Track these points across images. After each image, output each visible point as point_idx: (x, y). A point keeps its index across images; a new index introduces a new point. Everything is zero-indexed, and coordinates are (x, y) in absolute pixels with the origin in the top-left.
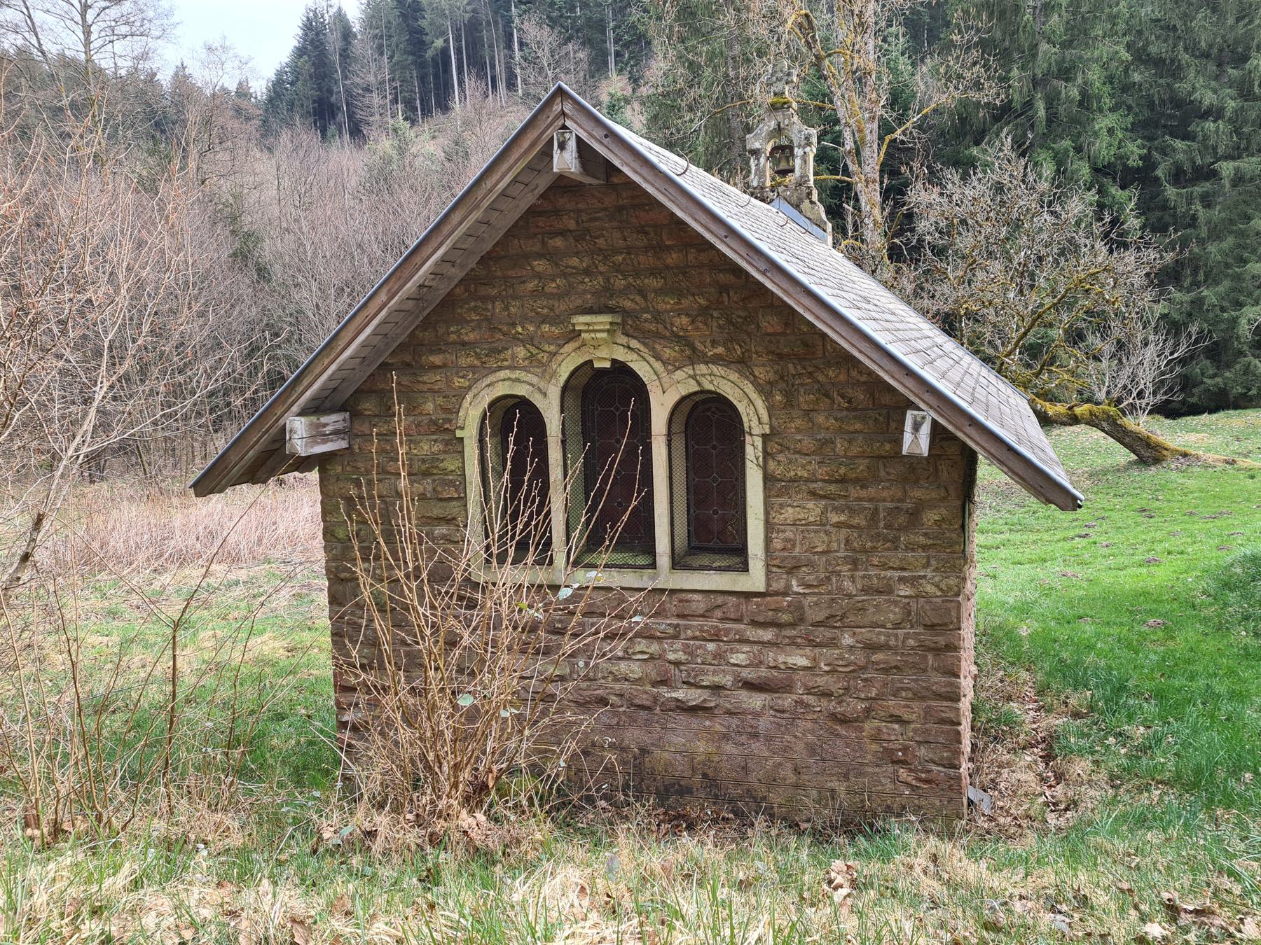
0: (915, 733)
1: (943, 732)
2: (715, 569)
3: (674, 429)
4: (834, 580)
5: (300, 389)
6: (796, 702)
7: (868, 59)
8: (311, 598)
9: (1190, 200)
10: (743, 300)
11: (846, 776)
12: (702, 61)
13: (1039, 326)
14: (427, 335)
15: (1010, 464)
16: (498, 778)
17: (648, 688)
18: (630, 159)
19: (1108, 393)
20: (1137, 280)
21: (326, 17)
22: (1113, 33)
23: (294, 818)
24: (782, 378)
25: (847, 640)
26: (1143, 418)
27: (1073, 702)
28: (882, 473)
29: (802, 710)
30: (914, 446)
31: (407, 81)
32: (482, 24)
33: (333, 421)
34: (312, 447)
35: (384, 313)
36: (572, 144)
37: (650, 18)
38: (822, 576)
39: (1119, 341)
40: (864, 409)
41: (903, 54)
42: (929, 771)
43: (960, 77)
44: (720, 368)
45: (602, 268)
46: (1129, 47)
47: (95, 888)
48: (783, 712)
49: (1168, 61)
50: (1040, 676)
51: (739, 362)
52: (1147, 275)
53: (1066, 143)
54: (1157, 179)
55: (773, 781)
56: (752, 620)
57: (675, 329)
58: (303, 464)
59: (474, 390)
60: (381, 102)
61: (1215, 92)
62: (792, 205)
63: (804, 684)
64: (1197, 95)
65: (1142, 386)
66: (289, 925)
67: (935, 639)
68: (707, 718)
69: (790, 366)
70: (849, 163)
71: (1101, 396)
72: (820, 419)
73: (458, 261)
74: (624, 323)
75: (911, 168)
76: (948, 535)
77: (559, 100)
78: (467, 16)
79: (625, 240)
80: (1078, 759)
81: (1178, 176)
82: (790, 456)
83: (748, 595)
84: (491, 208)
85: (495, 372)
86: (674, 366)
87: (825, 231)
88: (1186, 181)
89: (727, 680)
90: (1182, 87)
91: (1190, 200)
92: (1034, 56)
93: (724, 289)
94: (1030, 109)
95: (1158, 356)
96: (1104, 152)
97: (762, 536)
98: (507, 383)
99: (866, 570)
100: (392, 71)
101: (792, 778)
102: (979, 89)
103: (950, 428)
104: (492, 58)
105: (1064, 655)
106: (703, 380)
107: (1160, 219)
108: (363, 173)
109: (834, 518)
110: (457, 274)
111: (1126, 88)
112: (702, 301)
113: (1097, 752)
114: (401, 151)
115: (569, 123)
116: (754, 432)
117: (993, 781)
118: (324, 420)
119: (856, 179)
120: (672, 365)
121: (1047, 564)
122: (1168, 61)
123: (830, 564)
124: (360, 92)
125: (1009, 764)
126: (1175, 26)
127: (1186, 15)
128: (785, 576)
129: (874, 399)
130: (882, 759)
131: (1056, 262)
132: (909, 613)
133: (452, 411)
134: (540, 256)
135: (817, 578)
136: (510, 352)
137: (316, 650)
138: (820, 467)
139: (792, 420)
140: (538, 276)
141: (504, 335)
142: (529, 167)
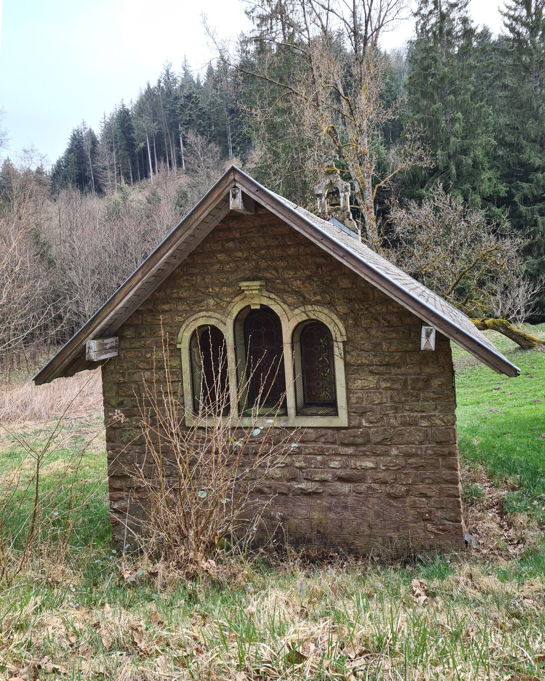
0: (435, 503)
1: (450, 502)
2: (320, 415)
3: (295, 340)
4: (385, 419)
6: (368, 487)
7: (365, 147)
8: (82, 438)
9: (533, 212)
10: (330, 271)
11: (398, 529)
12: (280, 151)
13: (464, 278)
14: (161, 295)
15: (479, 353)
16: (220, 539)
17: (285, 483)
18: (270, 202)
19: (502, 312)
20: (512, 253)
21: (83, 133)
22: (486, 132)
23: (102, 566)
24: (352, 311)
25: (394, 452)
26: (520, 325)
27: (510, 481)
28: (408, 360)
29: (371, 492)
30: (427, 345)
31: (125, 164)
33: (110, 341)
34: (100, 356)
35: (140, 284)
36: (239, 195)
37: (253, 130)
38: (379, 416)
39: (505, 285)
40: (397, 326)
41: (381, 144)
42: (444, 525)
43: (412, 155)
44: (319, 307)
45: (254, 257)
46: (495, 138)
47: (17, 614)
48: (360, 493)
49: (515, 144)
50: (489, 468)
51: (328, 304)
52: (517, 251)
53: (468, 186)
54: (515, 202)
55: (357, 534)
56: (341, 443)
57: (294, 287)
58: (91, 365)
59: (186, 323)
60: (112, 175)
61: (541, 159)
62: (340, 221)
63: (372, 478)
64: (532, 160)
65: (519, 308)
66: (130, 631)
67: (443, 449)
68: (318, 499)
69: (356, 305)
70: (358, 199)
71: (498, 314)
72: (374, 332)
73: (178, 256)
74: (266, 285)
75: (390, 201)
76: (446, 392)
77: (232, 173)
78: (156, 131)
79: (266, 242)
80: (519, 514)
81: (525, 201)
82: (358, 352)
83: (338, 429)
84: (196, 228)
85: (198, 313)
86: (294, 307)
87: (357, 234)
88: (530, 203)
89: (329, 477)
90: (524, 157)
91: (533, 212)
92: (448, 144)
93: (319, 266)
94: (448, 170)
95: (526, 292)
96: (487, 190)
97: (345, 396)
98: (204, 318)
99: (402, 412)
100: (118, 159)
101: (367, 531)
102: (421, 161)
103: (446, 335)
104: (169, 152)
105: (500, 455)
106: (310, 314)
107: (518, 222)
108: (104, 211)
109: (384, 385)
110: (177, 262)
111: (495, 158)
112: (308, 273)
113: (528, 509)
114: (125, 199)
115: (237, 185)
116: (338, 340)
117: (474, 528)
118: (106, 341)
119: (362, 207)
120: (293, 306)
121: (481, 404)
122: (515, 144)
123: (383, 410)
124: (101, 170)
125: (481, 519)
126: (517, 127)
127: (522, 122)
128: (358, 418)
129: (401, 321)
130: (417, 519)
131: (470, 245)
132: (427, 435)
133: (174, 335)
134: (221, 252)
135: (376, 418)
136: (205, 302)
137: (87, 468)
138: (374, 358)
139: (358, 333)
140: (220, 262)
141: (202, 293)
142: (216, 207)
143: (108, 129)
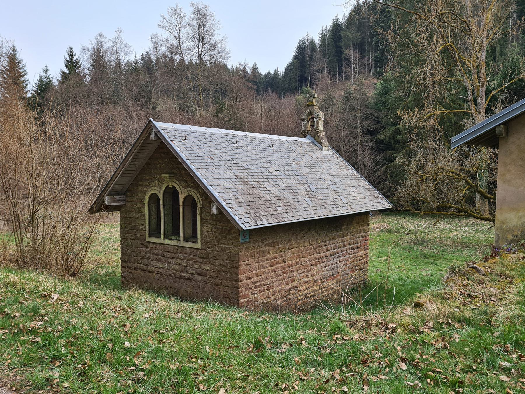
5: (107, 189)
21: (307, 43)
32: (366, 43)
33: (118, 197)
83: (198, 249)
89: (194, 272)
109: (214, 230)
143: (323, 39)
